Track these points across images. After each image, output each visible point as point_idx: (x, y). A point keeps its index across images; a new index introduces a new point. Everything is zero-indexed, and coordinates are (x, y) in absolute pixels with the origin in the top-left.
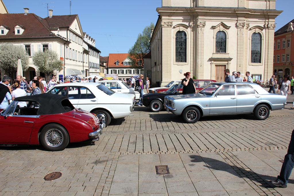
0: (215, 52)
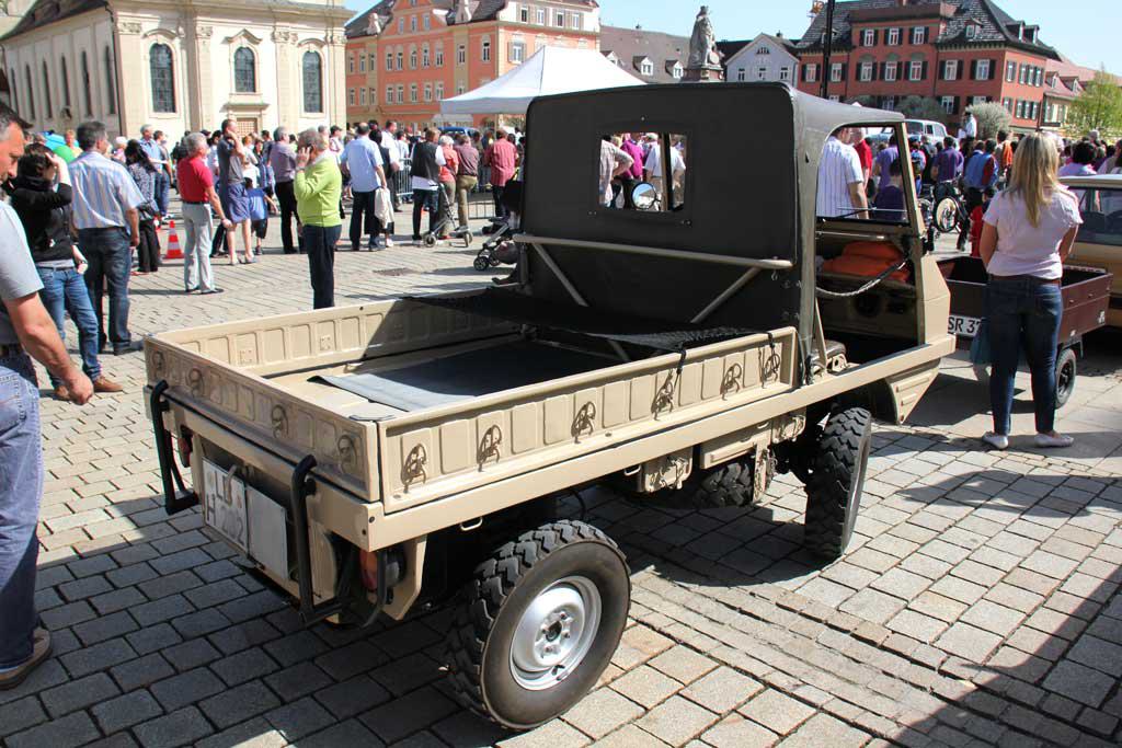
0: (234, 91)
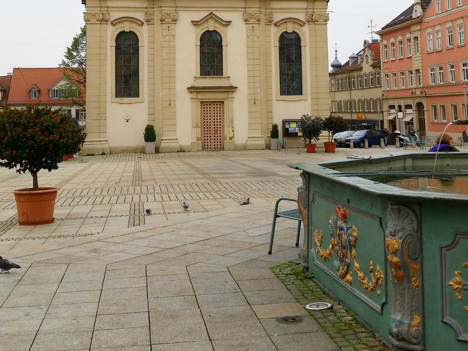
0: (199, 75)
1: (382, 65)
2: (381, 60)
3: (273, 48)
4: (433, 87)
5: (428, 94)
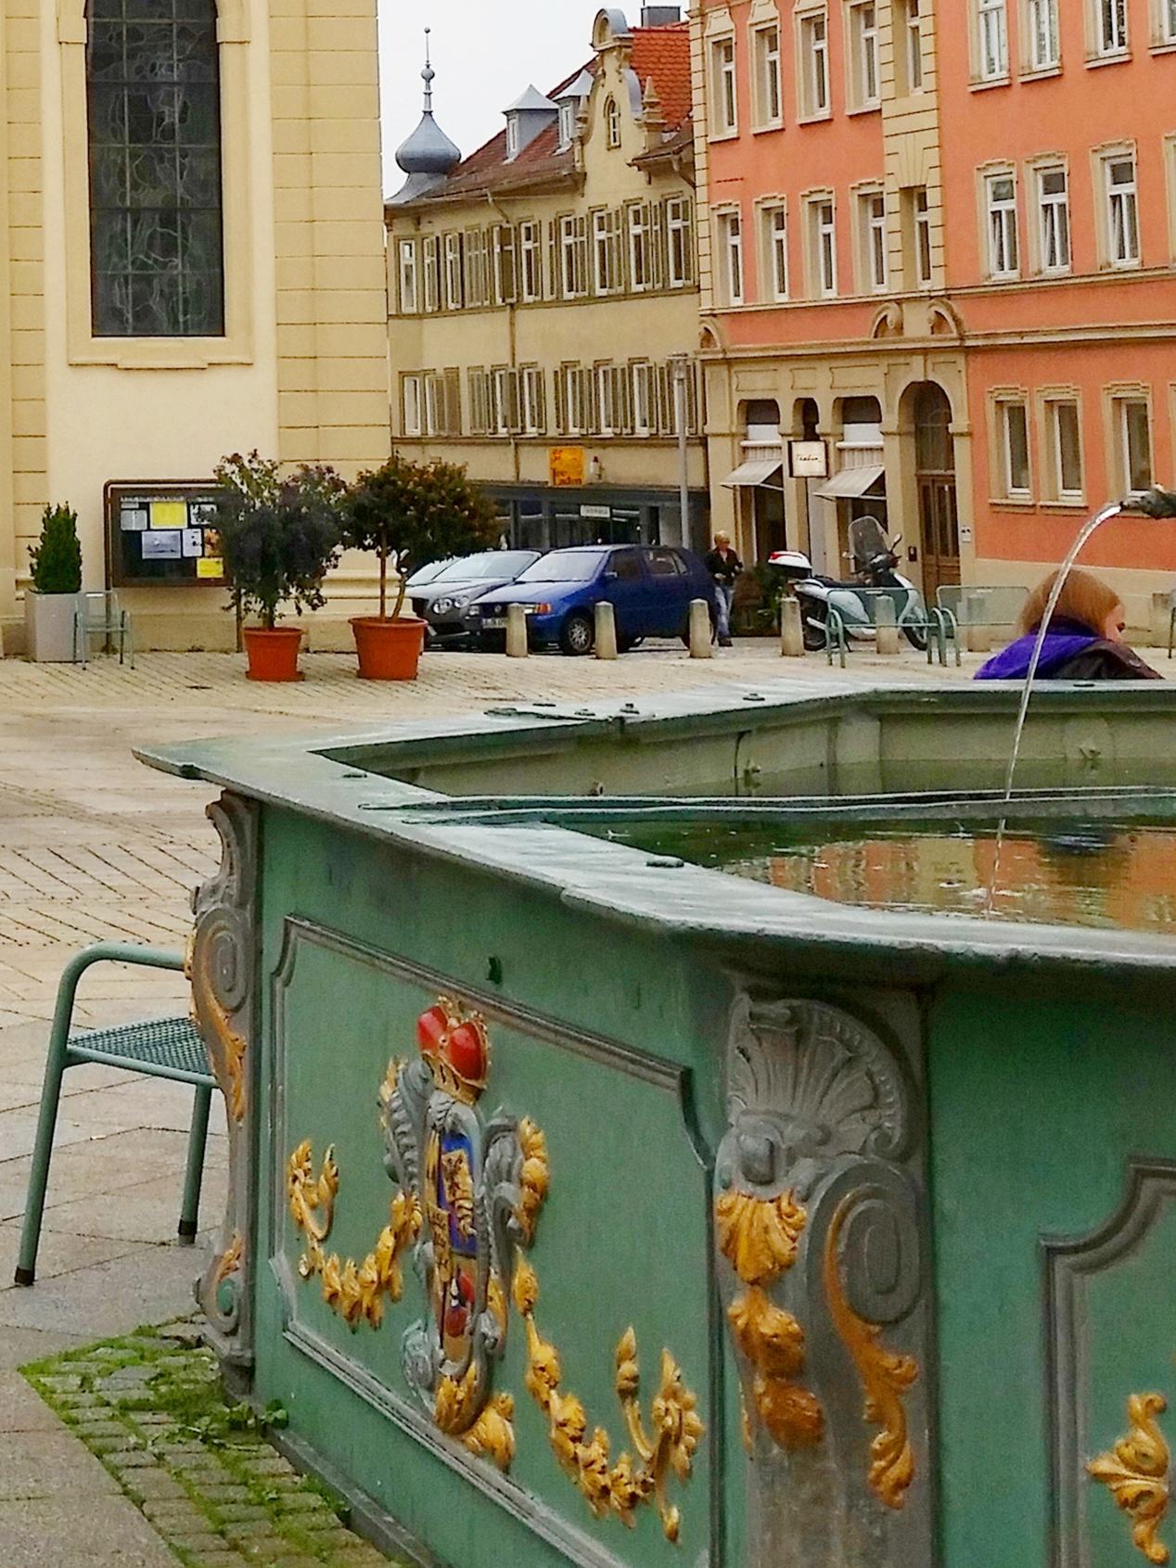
1: (700, 162)
2: (698, 129)
3: (50, 53)
4: (1003, 294)
5: (976, 337)
